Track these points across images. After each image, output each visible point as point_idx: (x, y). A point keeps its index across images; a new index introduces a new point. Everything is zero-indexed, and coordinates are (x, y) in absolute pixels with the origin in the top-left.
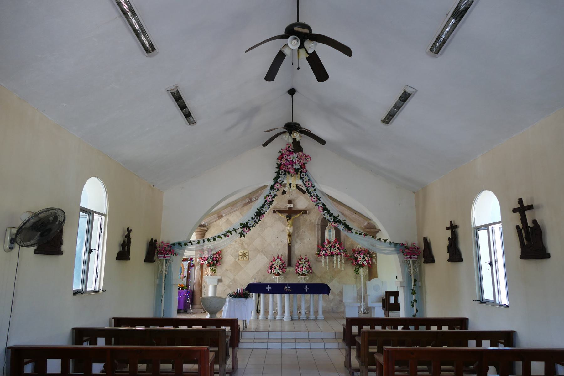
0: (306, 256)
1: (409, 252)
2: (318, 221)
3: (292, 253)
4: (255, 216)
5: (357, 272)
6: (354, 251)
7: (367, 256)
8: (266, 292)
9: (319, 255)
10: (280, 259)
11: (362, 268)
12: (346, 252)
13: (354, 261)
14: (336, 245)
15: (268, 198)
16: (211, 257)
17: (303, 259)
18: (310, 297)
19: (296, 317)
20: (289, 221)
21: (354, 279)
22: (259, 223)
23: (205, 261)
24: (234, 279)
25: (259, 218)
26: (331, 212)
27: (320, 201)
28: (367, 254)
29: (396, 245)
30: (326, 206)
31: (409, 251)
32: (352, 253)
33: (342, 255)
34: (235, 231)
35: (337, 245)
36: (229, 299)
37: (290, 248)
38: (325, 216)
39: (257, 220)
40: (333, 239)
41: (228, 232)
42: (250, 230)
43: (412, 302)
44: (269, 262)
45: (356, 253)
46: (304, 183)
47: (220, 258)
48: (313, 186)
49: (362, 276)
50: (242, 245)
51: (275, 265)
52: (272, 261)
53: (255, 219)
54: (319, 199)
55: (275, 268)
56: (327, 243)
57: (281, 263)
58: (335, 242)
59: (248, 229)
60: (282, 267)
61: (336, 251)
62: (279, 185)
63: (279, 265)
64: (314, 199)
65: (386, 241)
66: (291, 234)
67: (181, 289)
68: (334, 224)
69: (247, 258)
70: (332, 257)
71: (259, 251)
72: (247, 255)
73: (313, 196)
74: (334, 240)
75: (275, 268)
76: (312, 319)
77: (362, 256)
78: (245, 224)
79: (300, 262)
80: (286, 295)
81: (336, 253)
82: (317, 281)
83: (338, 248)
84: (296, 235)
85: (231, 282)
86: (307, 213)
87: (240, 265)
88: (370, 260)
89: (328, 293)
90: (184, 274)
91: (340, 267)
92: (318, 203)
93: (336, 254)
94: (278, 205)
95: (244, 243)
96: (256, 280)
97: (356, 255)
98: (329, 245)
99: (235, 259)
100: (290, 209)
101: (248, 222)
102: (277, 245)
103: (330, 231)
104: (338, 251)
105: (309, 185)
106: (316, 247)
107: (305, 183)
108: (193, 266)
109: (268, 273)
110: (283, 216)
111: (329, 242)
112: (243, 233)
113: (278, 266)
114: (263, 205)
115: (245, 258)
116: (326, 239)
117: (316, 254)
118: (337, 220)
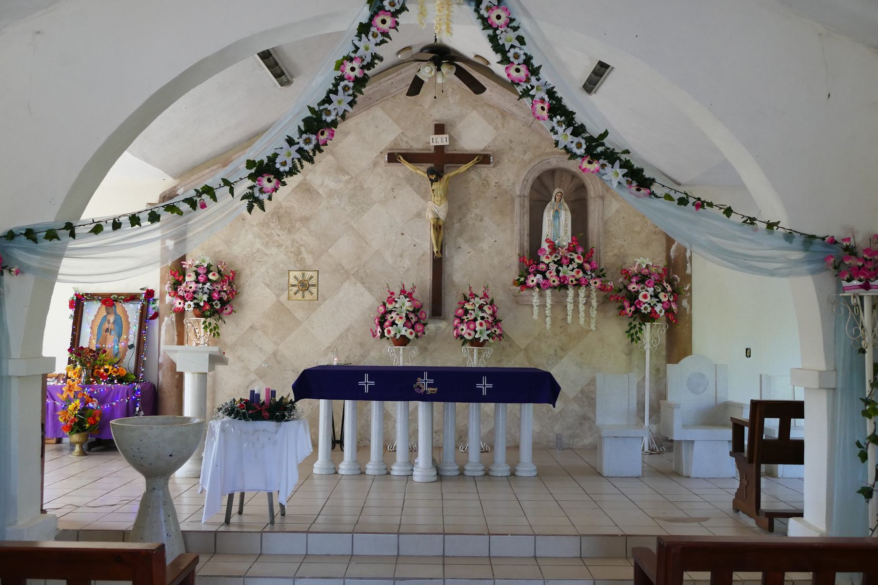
0: (486, 288)
1: (859, 268)
2: (524, 187)
3: (445, 277)
4: (301, 133)
5: (634, 337)
6: (626, 274)
7: (664, 290)
8: (357, 394)
9: (523, 285)
10: (409, 296)
11: (648, 325)
12: (603, 279)
13: (626, 304)
14: (575, 256)
15: (349, 65)
16: (206, 290)
17: (476, 296)
18: (496, 409)
19: (451, 469)
20: (436, 186)
21: (624, 356)
22: (315, 158)
23: (186, 301)
24: (275, 354)
25: (314, 142)
26: (579, 119)
27: (538, 80)
28: (665, 284)
29: (811, 243)
30: (559, 100)
31: (860, 264)
32: (621, 280)
33: (593, 287)
34: (227, 188)
35: (579, 258)
36: (223, 423)
37: (438, 264)
38: (556, 133)
39: (306, 148)
40: (565, 238)
41: (203, 192)
42: (284, 184)
43: (858, 444)
44: (379, 304)
45: (634, 280)
46: (483, 12)
47: (234, 293)
48: (514, 24)
49: (647, 347)
50: (298, 255)
51: (394, 315)
52: (385, 301)
53: (302, 145)
54: (535, 71)
55: (393, 324)
56: (547, 249)
57: (411, 309)
58: (572, 249)
59: (274, 181)
60: (413, 320)
61: (574, 273)
62: (389, 21)
63: (404, 315)
64: (518, 70)
65: (775, 228)
66: (441, 223)
67: (116, 382)
68: (590, 163)
69: (312, 294)
70: (563, 291)
71: (347, 272)
72: (313, 285)
73: (512, 59)
74: (570, 241)
75: (393, 324)
76: (500, 474)
77: (652, 289)
78: (266, 161)
79: (467, 306)
80: (421, 407)
81: (573, 279)
82: (516, 361)
83: (580, 266)
84: (457, 226)
85: (265, 362)
86: (489, 163)
87: (291, 313)
88: (673, 301)
89: (552, 401)
90: (127, 340)
91: (585, 321)
92: (533, 87)
93: (575, 282)
94: (405, 139)
95: (302, 248)
96: (337, 356)
97: (634, 285)
98: (552, 258)
99: (278, 296)
100: (439, 149)
101: (276, 155)
102: (401, 256)
103: (556, 215)
104: (581, 274)
105: (501, 22)
106: (515, 260)
107: (486, 15)
108: (156, 315)
109: (374, 336)
110: (418, 171)
111: (554, 248)
112: (257, 194)
113: (401, 318)
114: (330, 91)
115: (307, 293)
116: (544, 238)
117: (514, 284)
118: (600, 149)
